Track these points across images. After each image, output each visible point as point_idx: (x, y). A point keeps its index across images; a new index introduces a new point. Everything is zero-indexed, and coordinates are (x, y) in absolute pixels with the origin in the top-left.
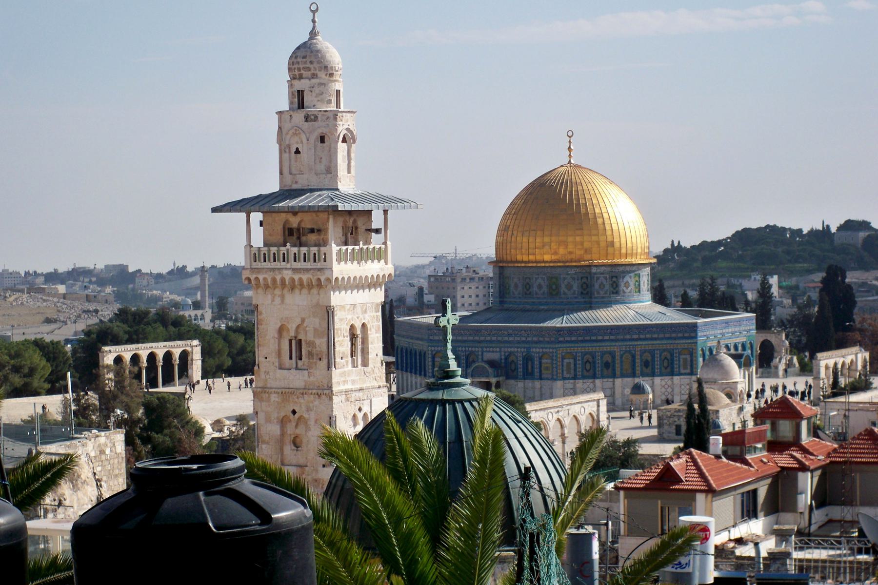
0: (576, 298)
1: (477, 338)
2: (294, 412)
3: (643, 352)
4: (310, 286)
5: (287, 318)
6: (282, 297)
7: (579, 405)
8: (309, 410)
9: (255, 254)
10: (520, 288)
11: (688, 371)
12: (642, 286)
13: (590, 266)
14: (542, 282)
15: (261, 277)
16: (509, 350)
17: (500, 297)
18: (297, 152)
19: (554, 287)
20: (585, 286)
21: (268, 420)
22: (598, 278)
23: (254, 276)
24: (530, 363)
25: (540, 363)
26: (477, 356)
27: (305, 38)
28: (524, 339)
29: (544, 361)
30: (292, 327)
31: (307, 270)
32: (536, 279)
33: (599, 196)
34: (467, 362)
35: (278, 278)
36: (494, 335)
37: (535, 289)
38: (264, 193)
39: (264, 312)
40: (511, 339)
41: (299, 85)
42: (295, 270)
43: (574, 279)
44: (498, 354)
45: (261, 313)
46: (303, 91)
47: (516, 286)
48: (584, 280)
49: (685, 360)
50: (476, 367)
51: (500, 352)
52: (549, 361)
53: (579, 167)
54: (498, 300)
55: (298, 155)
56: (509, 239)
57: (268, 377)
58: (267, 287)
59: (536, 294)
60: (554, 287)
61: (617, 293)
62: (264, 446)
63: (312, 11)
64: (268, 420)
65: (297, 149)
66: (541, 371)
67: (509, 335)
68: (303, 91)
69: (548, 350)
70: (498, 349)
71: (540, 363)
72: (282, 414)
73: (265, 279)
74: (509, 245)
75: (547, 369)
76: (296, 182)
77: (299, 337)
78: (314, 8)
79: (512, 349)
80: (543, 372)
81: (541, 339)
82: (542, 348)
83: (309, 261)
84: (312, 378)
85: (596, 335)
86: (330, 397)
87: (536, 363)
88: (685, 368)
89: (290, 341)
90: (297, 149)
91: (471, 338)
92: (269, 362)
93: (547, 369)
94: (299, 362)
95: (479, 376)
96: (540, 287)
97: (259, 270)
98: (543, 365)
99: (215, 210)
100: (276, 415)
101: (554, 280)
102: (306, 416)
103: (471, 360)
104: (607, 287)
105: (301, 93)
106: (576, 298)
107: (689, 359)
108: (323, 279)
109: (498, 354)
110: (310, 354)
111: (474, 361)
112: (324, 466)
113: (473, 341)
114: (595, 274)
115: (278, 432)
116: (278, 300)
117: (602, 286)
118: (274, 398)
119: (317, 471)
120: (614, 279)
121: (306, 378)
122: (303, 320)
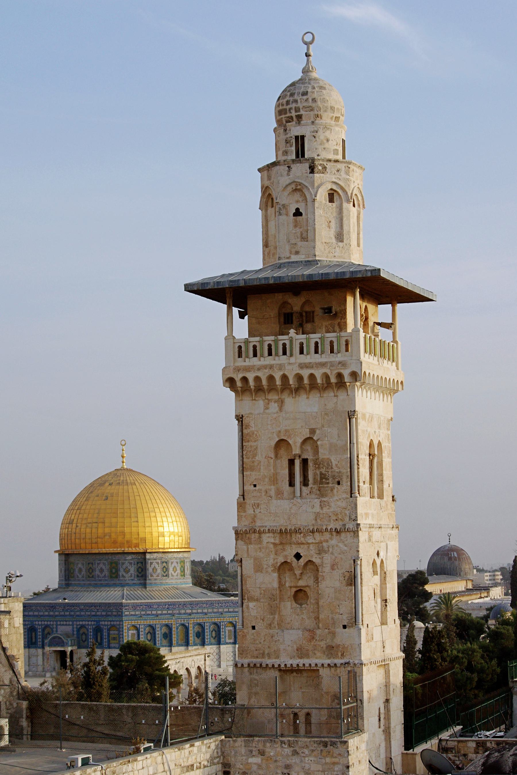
0: (132, 580)
1: (51, 613)
2: (298, 556)
3: (195, 624)
4: (327, 385)
5: (286, 431)
6: (281, 402)
7: (191, 658)
8: (321, 551)
9: (240, 347)
10: (84, 572)
11: (232, 641)
12: (186, 571)
13: (144, 553)
14: (104, 567)
15: (251, 377)
16: (81, 623)
17: (66, 580)
18: (298, 213)
19: (114, 570)
20: (140, 570)
21: (258, 568)
22: (151, 563)
23: (240, 376)
24: (99, 634)
25: (109, 634)
26: (52, 629)
27: (299, 75)
28: (93, 613)
29: (111, 632)
30: (296, 442)
31: (323, 365)
32: (98, 564)
33: (150, 494)
34: (43, 634)
35: (278, 376)
36: (67, 610)
37: (97, 572)
38: (248, 269)
39: (252, 424)
40: (83, 613)
41: (296, 130)
42: (302, 366)
43: (131, 563)
44: (71, 627)
45: (248, 426)
46: (303, 137)
47: (80, 570)
48: (140, 565)
49: (230, 631)
50: (54, 638)
51: (73, 625)
52: (116, 632)
53: (132, 470)
54: (64, 582)
55: (299, 218)
56: (74, 530)
57: (257, 511)
58: (259, 389)
59: (98, 576)
60: (114, 570)
61: (167, 576)
62: (251, 605)
63: (306, 43)
64: (258, 568)
65: (297, 210)
66: (109, 641)
67: (81, 610)
68: (303, 137)
69: (115, 623)
70: (71, 623)
71: (109, 634)
72: (281, 560)
73: (257, 379)
74: (73, 535)
75: (114, 639)
76: (297, 253)
77: (305, 456)
78: (308, 38)
79: (84, 623)
80: (111, 641)
81: (109, 613)
82: (111, 621)
83: (323, 352)
84: (325, 510)
85: (156, 609)
86: (355, 532)
87: (105, 634)
88: (229, 639)
89: (291, 462)
90: (297, 210)
91: (46, 613)
92: (260, 491)
93: (114, 639)
94: (304, 488)
95: (57, 645)
96: (102, 571)
97: (248, 369)
98: (111, 636)
99: (190, 288)
100: (271, 562)
101: (114, 565)
102: (316, 560)
103: (46, 632)
104: (159, 571)
105: (300, 140)
106: (132, 580)
107: (233, 630)
108: (346, 373)
109: (71, 627)
110: (323, 478)
111: (49, 633)
112: (345, 627)
113: (49, 616)
114: (149, 559)
115: (276, 585)
116: (274, 407)
117: (155, 569)
118: (267, 538)
119: (333, 634)
120: (165, 564)
121: (317, 509)
122: (313, 431)
